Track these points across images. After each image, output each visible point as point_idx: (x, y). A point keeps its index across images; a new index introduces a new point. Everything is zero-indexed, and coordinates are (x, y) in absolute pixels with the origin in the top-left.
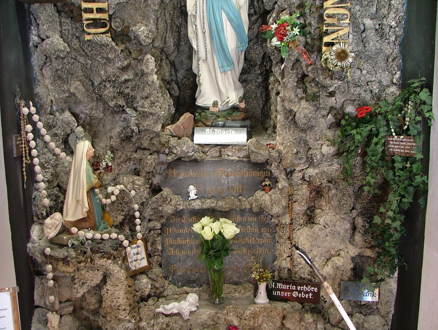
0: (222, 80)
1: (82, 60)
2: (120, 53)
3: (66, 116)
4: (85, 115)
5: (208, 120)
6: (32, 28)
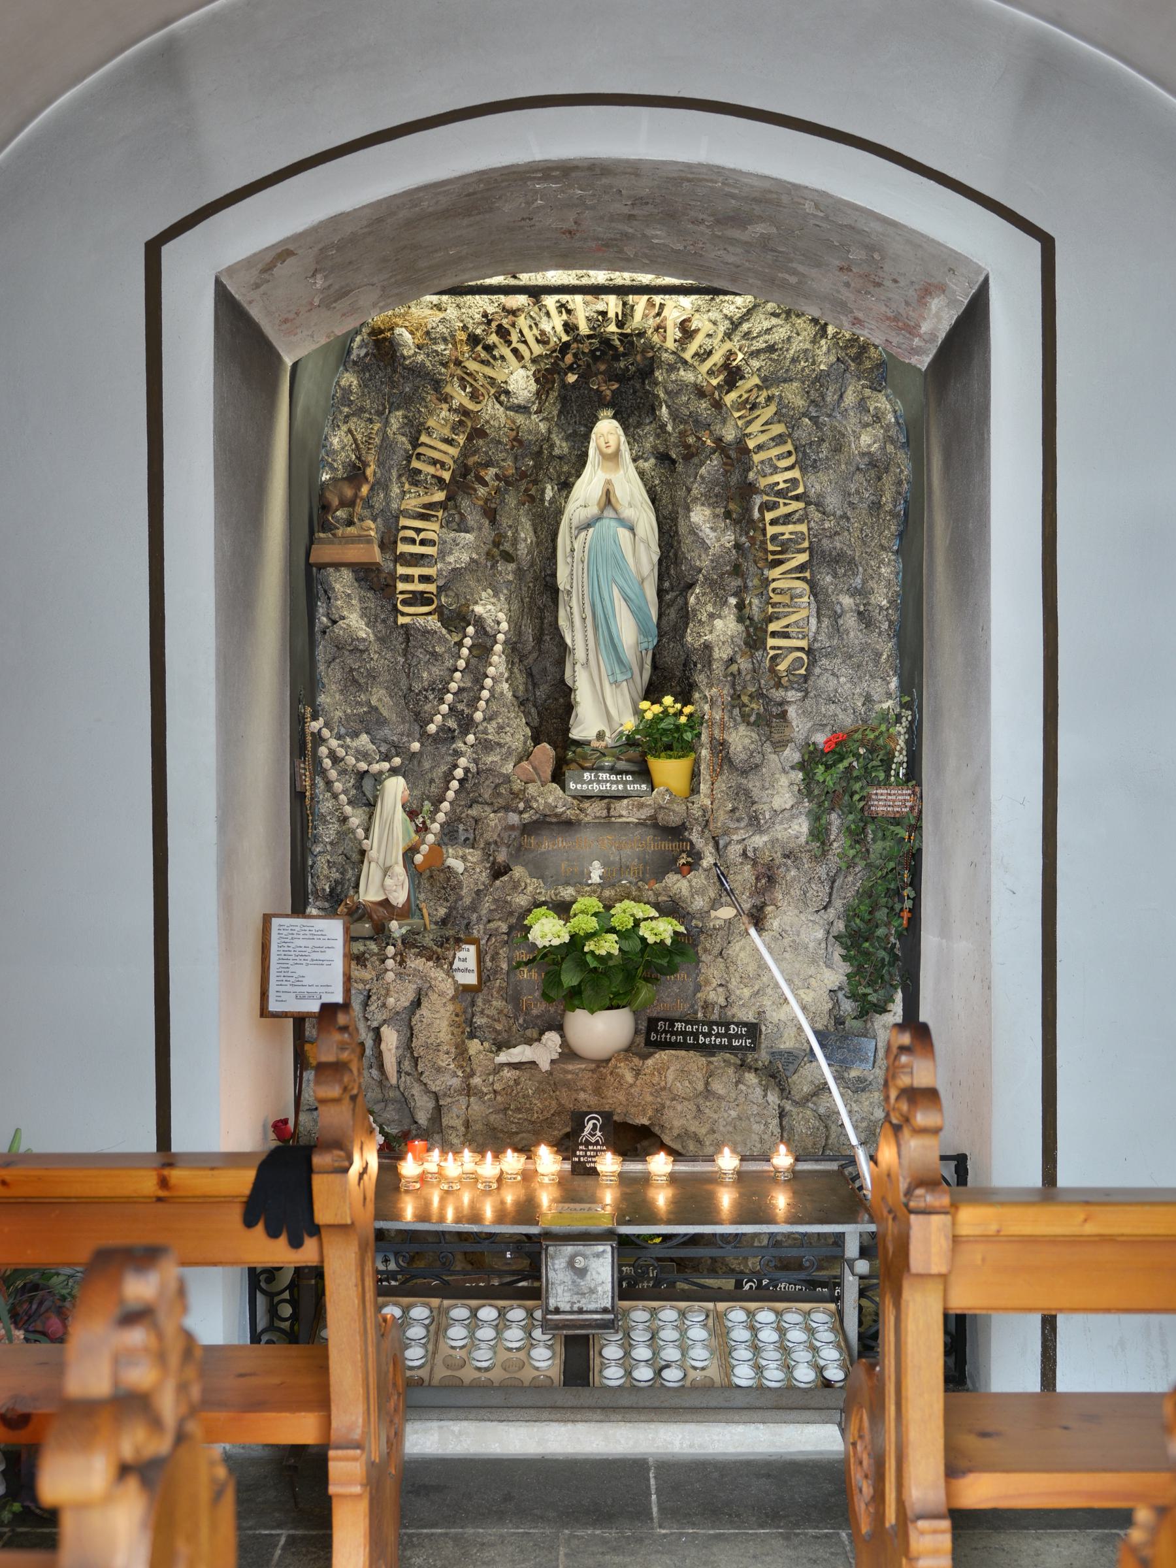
6: (319, 603)
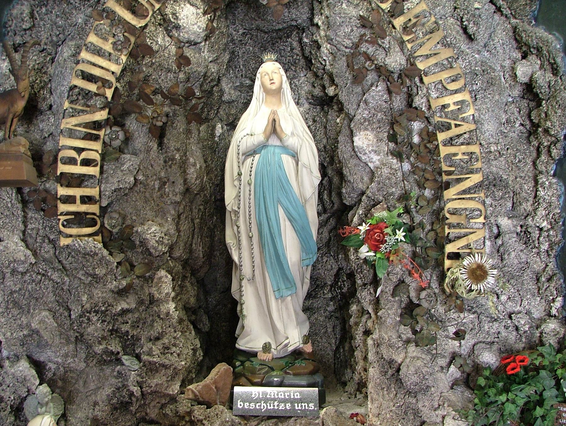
0: (278, 310)
1: (55, 276)
2: (114, 268)
3: (21, 368)
4: (56, 365)
5: (255, 374)
